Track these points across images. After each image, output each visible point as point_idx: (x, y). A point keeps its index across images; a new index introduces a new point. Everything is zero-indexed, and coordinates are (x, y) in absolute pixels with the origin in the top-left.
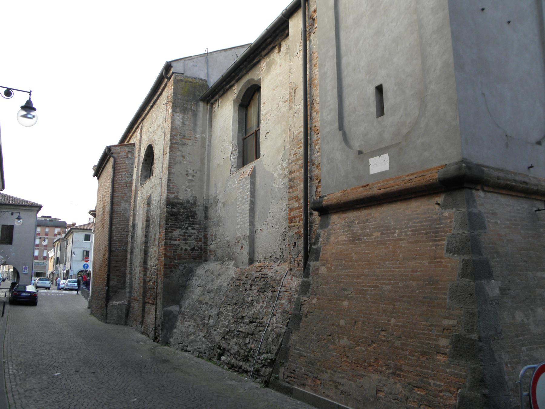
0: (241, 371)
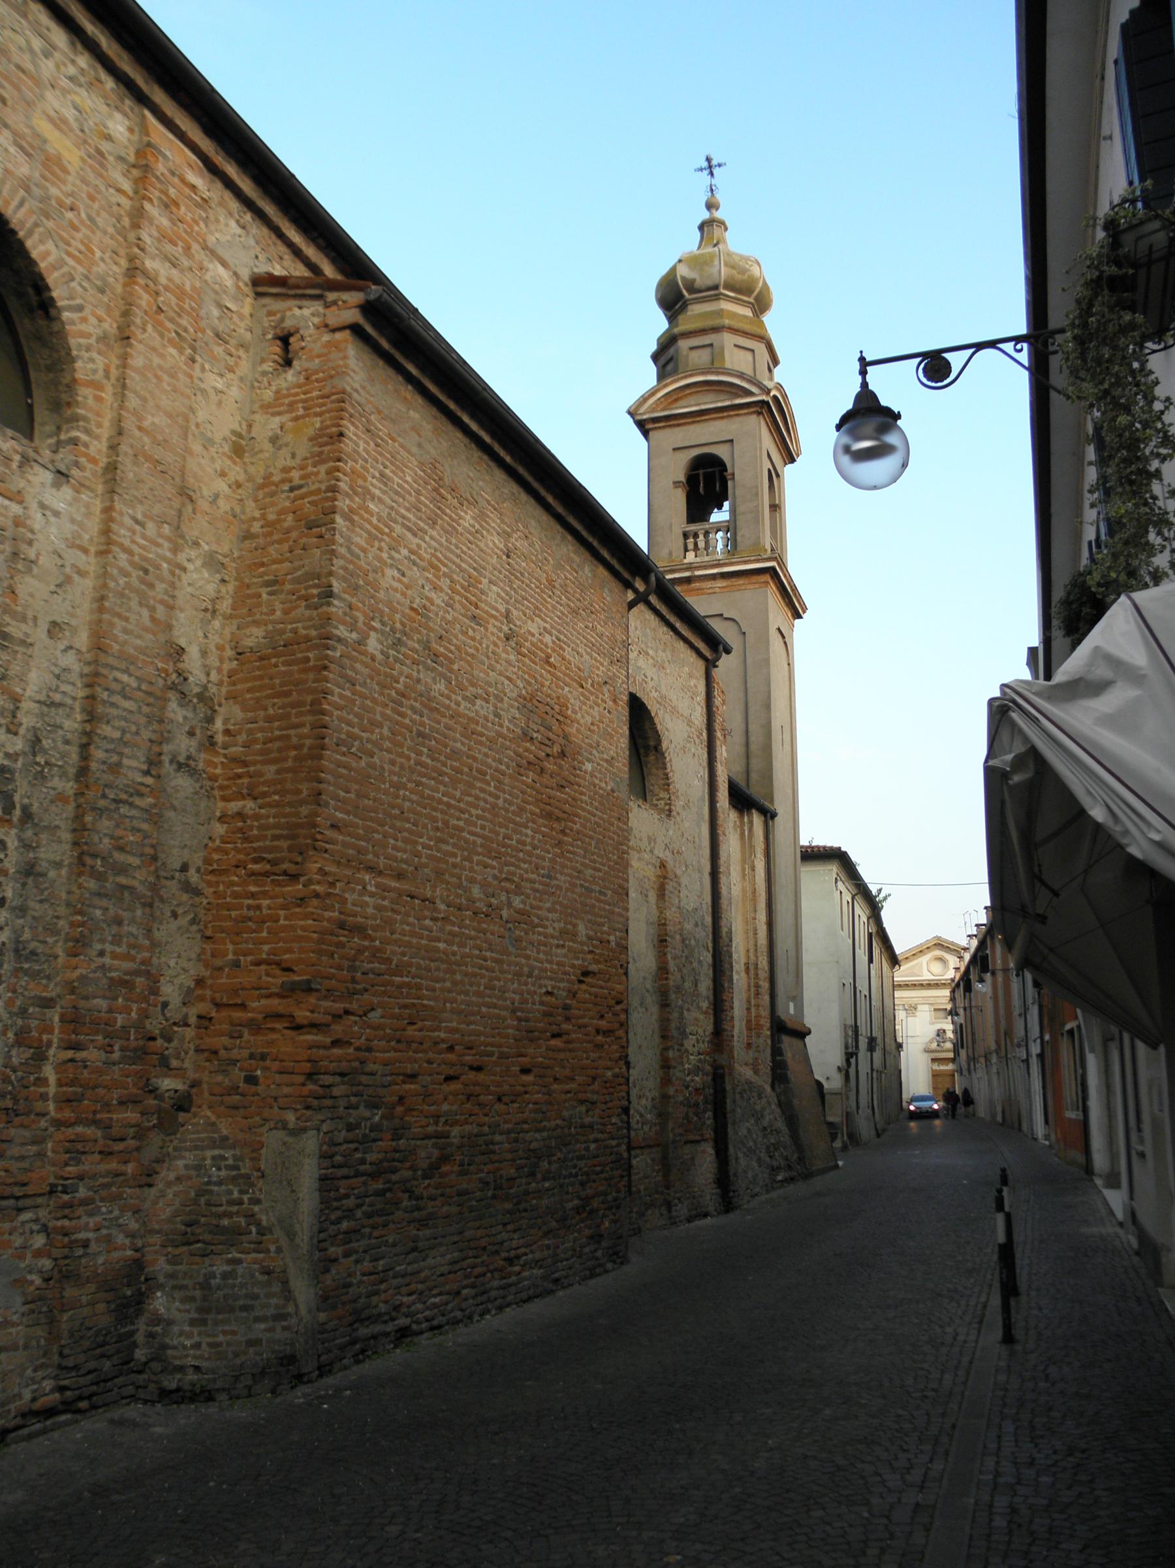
0: (792, 1179)
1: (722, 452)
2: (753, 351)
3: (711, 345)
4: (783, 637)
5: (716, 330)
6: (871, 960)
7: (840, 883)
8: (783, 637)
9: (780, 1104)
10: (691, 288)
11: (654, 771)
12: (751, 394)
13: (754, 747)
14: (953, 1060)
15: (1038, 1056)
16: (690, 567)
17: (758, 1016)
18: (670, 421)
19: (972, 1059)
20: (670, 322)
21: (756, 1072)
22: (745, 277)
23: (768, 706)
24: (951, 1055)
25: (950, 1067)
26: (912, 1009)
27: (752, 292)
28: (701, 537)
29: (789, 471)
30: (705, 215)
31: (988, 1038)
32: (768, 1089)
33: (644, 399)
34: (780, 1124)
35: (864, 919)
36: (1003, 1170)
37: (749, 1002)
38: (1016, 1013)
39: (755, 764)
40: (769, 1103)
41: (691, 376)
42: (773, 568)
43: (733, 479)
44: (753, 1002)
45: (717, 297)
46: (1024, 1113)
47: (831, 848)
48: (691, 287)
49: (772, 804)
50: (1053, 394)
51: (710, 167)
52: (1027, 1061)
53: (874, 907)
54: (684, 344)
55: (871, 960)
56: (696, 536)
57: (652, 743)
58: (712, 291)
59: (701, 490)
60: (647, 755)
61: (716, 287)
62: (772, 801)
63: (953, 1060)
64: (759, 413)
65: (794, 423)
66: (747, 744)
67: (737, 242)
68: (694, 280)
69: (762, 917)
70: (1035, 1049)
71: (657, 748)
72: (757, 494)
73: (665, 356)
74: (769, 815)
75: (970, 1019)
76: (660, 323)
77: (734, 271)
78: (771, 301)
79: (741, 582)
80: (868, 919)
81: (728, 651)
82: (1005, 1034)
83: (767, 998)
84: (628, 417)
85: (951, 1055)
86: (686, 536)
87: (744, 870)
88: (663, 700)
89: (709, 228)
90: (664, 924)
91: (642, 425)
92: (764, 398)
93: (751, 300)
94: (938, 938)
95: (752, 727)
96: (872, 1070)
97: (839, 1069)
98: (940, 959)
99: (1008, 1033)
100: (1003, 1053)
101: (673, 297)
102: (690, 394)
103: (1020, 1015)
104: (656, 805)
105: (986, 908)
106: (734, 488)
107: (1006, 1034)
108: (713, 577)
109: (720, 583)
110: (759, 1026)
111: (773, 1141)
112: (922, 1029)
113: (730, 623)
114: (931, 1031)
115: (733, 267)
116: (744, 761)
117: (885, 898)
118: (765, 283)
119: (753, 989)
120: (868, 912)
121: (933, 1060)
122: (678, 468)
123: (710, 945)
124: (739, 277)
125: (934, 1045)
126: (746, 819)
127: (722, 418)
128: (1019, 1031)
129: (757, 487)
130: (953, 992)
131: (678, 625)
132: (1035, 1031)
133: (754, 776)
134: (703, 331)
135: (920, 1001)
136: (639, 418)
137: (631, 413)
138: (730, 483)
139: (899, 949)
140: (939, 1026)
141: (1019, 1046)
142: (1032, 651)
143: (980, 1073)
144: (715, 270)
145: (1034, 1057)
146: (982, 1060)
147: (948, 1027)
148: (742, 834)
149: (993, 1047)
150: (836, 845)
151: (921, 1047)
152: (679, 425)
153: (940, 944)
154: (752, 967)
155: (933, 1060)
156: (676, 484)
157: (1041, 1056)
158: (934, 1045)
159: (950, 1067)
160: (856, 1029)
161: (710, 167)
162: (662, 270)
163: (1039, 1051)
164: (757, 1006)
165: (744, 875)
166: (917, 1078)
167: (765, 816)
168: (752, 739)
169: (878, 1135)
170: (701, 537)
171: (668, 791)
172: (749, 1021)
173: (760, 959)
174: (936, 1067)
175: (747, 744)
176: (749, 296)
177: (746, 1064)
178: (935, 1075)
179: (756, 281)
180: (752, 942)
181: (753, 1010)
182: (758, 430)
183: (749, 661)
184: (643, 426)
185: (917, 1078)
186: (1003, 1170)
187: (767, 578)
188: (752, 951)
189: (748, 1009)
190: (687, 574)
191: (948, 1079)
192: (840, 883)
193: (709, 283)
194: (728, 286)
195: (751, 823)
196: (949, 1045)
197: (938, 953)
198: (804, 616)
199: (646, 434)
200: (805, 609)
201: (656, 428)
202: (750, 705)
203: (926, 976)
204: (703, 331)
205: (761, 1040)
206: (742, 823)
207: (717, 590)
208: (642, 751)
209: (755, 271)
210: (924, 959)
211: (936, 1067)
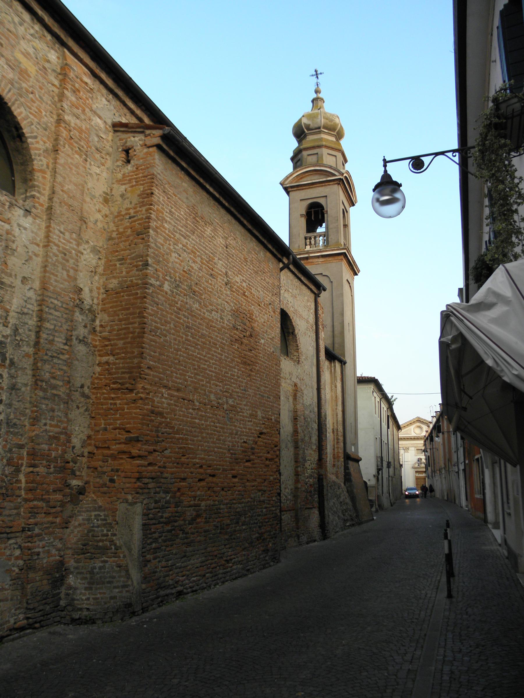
0: (353, 525)
1: (322, 201)
2: (336, 156)
3: (317, 154)
4: (349, 284)
5: (319, 147)
6: (388, 427)
7: (374, 393)
8: (349, 284)
9: (348, 492)
10: (308, 128)
11: (292, 343)
12: (335, 175)
13: (336, 333)
14: (425, 472)
15: (463, 470)
16: (308, 252)
17: (338, 452)
18: (299, 187)
19: (434, 471)
20: (299, 144)
21: (337, 477)
22: (332, 123)
23: (342, 314)
24: (424, 470)
25: (424, 475)
26: (407, 449)
27: (336, 130)
28: (313, 239)
29: (352, 210)
30: (315, 96)
31: (441, 462)
32: (343, 485)
33: (287, 178)
34: (348, 500)
35: (385, 409)
36: (447, 521)
37: (334, 446)
38: (453, 451)
39: (337, 340)
40: (343, 491)
41: (308, 167)
42: (345, 253)
43: (327, 213)
44: (336, 446)
45: (320, 132)
46: (457, 496)
47: (371, 378)
48: (308, 128)
49: (344, 358)
50: (470, 175)
51: (317, 74)
52: (458, 473)
53: (390, 404)
54: (305, 153)
55: (388, 427)
56: (310, 238)
57: (291, 331)
58: (318, 130)
59: (313, 218)
60: (288, 336)
61: (319, 128)
62: (344, 357)
63: (425, 472)
64: (339, 184)
65: (354, 188)
66: (333, 331)
67: (329, 108)
68: (310, 125)
69: (340, 408)
70: (462, 467)
71: (293, 333)
72: (338, 220)
73: (297, 159)
74: (343, 363)
75: (433, 454)
76: (294, 144)
77: (327, 121)
78: (344, 134)
79: (331, 259)
80: (387, 409)
81: (325, 290)
82: (448, 460)
83: (342, 444)
84: (280, 185)
85: (424, 470)
86: (306, 238)
87: (332, 387)
88: (295, 312)
89: (316, 101)
90: (296, 412)
91: (286, 189)
92: (341, 177)
93: (335, 134)
94: (418, 418)
95: (335, 324)
96: (389, 476)
97: (374, 476)
98: (419, 427)
99: (450, 460)
100: (447, 469)
101: (300, 132)
102: (308, 175)
103: (455, 452)
104: (293, 358)
105: (440, 404)
106: (327, 217)
107: (448, 460)
108: (318, 257)
109: (321, 260)
110: (339, 457)
111: (345, 508)
112: (411, 458)
113: (326, 277)
114: (415, 459)
115: (327, 119)
116: (332, 339)
117: (395, 400)
118: (341, 126)
119: (336, 440)
120: (387, 406)
121: (416, 472)
122: (302, 208)
123: (317, 421)
124: (329, 123)
125: (417, 465)
126: (333, 365)
127: (322, 186)
128: (455, 459)
129: (337, 217)
130: (425, 441)
131: (302, 278)
132: (462, 459)
133: (336, 346)
134: (313, 148)
135: (410, 445)
136: (285, 186)
137: (281, 184)
138: (325, 215)
139: (401, 423)
140: (419, 457)
141: (454, 465)
142: (460, 290)
143: (437, 478)
144: (319, 120)
145: (461, 471)
146: (438, 472)
147: (423, 457)
148: (331, 371)
149: (443, 466)
150: (373, 376)
151: (411, 466)
152: (303, 189)
153: (419, 420)
154: (335, 431)
155: (416, 472)
156: (302, 215)
157: (464, 470)
158: (417, 465)
159: (424, 475)
160: (382, 458)
161: (317, 74)
162: (295, 120)
163: (463, 468)
164: (338, 448)
165: (332, 390)
166: (409, 480)
167: (341, 363)
168: (336, 329)
169: (392, 505)
170: (313, 239)
171: (298, 352)
172: (334, 455)
173: (339, 427)
174: (417, 475)
175: (333, 331)
176: (334, 132)
177: (333, 474)
178: (417, 479)
179: (337, 125)
180: (335, 419)
181: (336, 449)
182: (338, 191)
183: (334, 294)
184: (287, 190)
185: (409, 480)
186: (447, 521)
187: (342, 257)
188: (335, 423)
189: (334, 449)
190: (306, 256)
191: (423, 480)
192: (374, 393)
193: (316, 126)
194: (325, 127)
195: (335, 366)
196: (423, 465)
197: (418, 424)
198: (359, 274)
199: (288, 193)
200: (359, 271)
201: (292, 191)
202: (334, 314)
203: (413, 435)
204: (313, 148)
205: (339, 463)
206: (331, 366)
207: (320, 263)
208: (286, 334)
209: (337, 120)
210: (412, 427)
211: (417, 475)
